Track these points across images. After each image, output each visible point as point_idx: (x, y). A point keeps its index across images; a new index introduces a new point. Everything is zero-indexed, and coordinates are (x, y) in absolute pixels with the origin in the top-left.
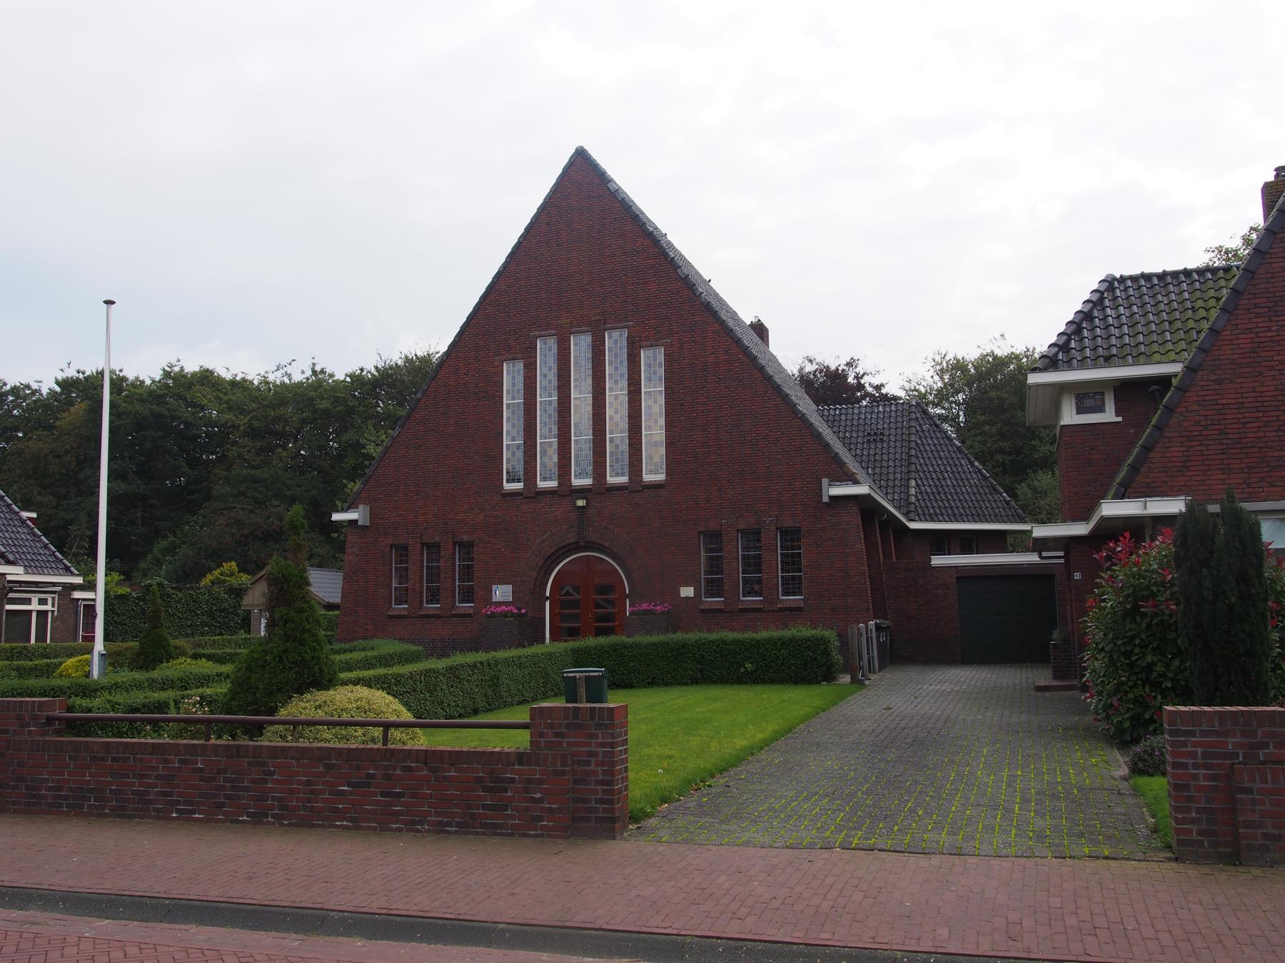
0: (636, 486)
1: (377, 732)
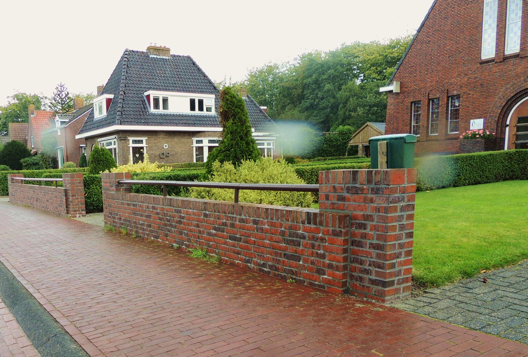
1: (231, 193)
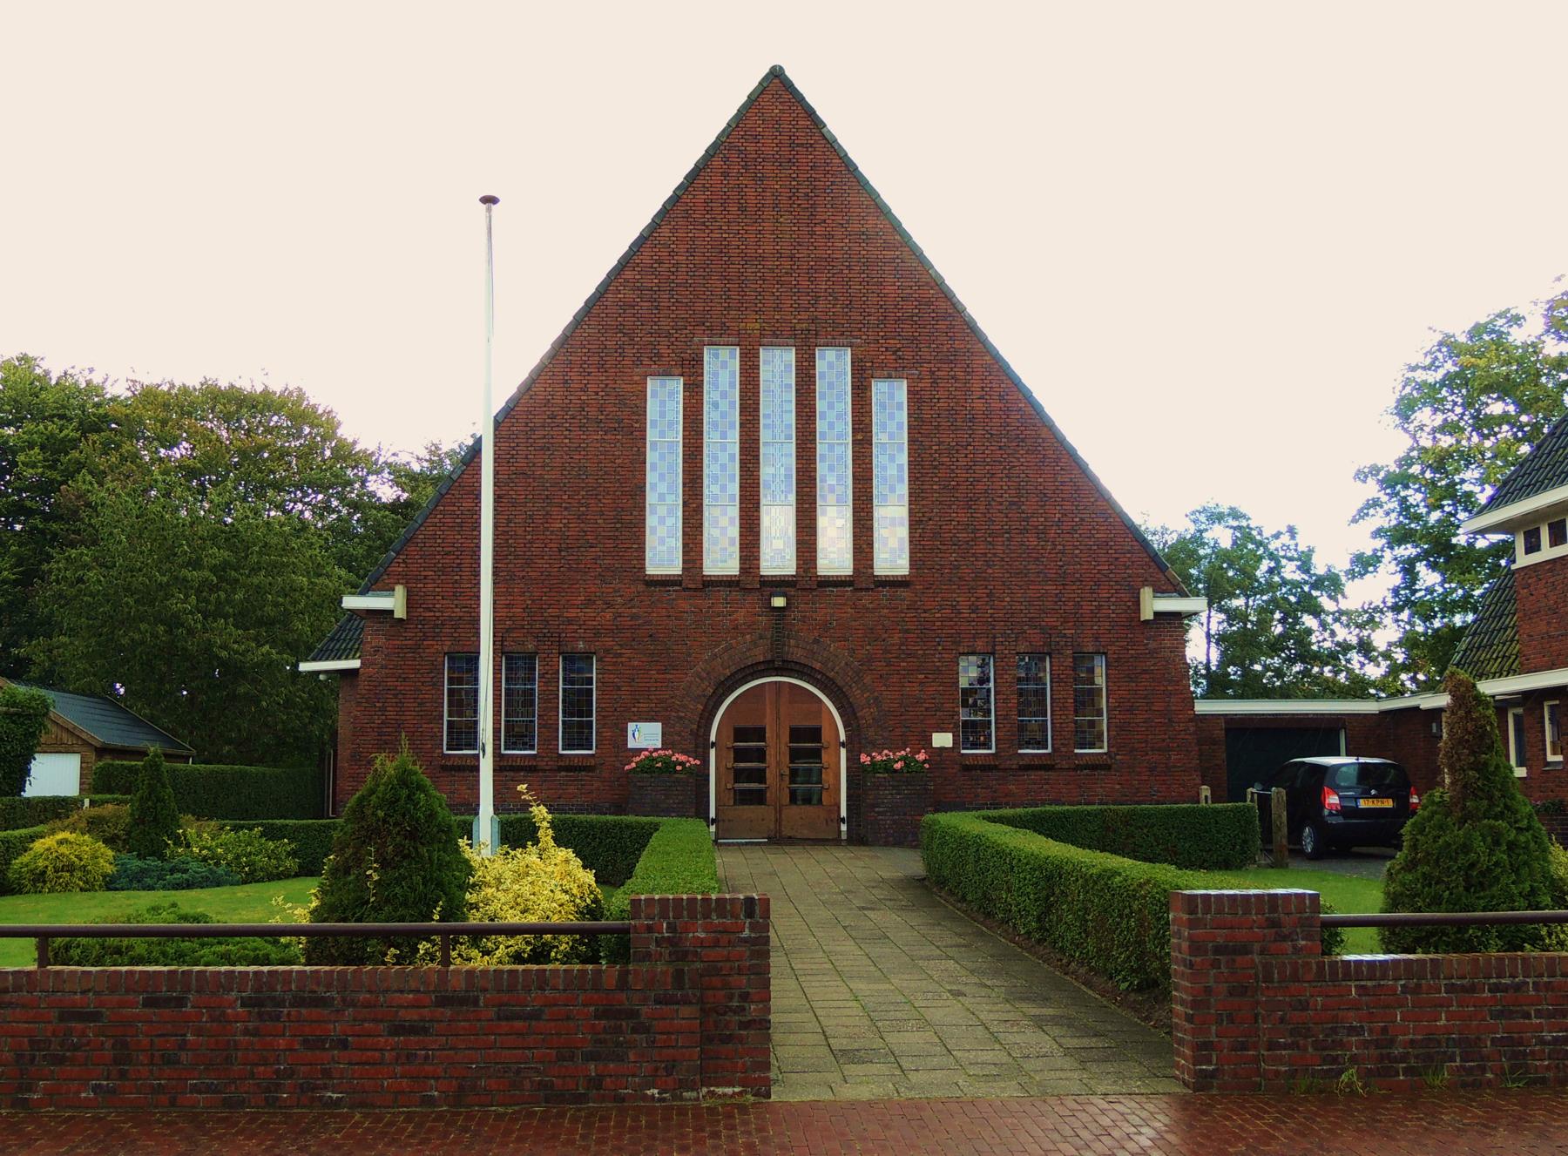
0: (863, 577)
